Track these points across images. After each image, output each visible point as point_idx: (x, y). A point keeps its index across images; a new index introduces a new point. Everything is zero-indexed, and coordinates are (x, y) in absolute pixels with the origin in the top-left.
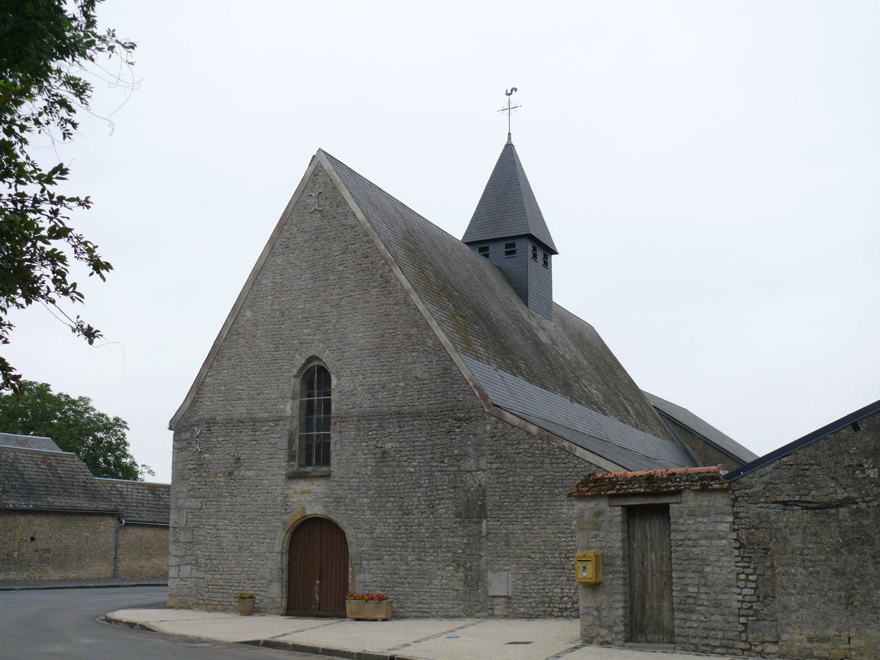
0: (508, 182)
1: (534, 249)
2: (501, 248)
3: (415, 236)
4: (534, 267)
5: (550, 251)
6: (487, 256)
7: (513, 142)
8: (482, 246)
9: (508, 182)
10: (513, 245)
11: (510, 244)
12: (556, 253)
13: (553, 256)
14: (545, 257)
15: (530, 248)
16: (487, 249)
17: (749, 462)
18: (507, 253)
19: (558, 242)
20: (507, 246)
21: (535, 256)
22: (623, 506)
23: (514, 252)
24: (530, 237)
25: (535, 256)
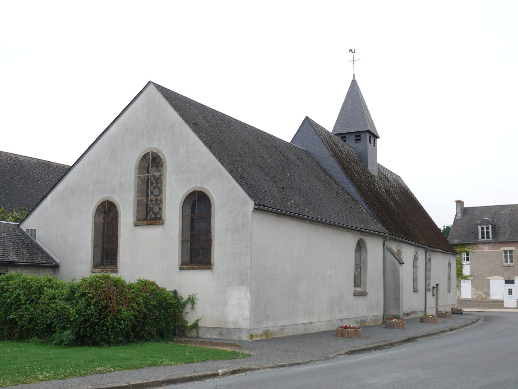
0: (354, 100)
1: (370, 137)
2: (353, 137)
3: (439, 230)
4: (370, 146)
5: (376, 137)
6: (345, 141)
7: (356, 78)
8: (342, 136)
9: (354, 100)
10: (359, 136)
11: (358, 136)
12: (378, 138)
13: (378, 139)
14: (374, 140)
15: (368, 137)
16: (345, 137)
17: (378, 162)
18: (356, 140)
19: (380, 133)
20: (356, 136)
21: (370, 141)
22: (505, 308)
23: (360, 140)
24: (369, 132)
25: (370, 141)
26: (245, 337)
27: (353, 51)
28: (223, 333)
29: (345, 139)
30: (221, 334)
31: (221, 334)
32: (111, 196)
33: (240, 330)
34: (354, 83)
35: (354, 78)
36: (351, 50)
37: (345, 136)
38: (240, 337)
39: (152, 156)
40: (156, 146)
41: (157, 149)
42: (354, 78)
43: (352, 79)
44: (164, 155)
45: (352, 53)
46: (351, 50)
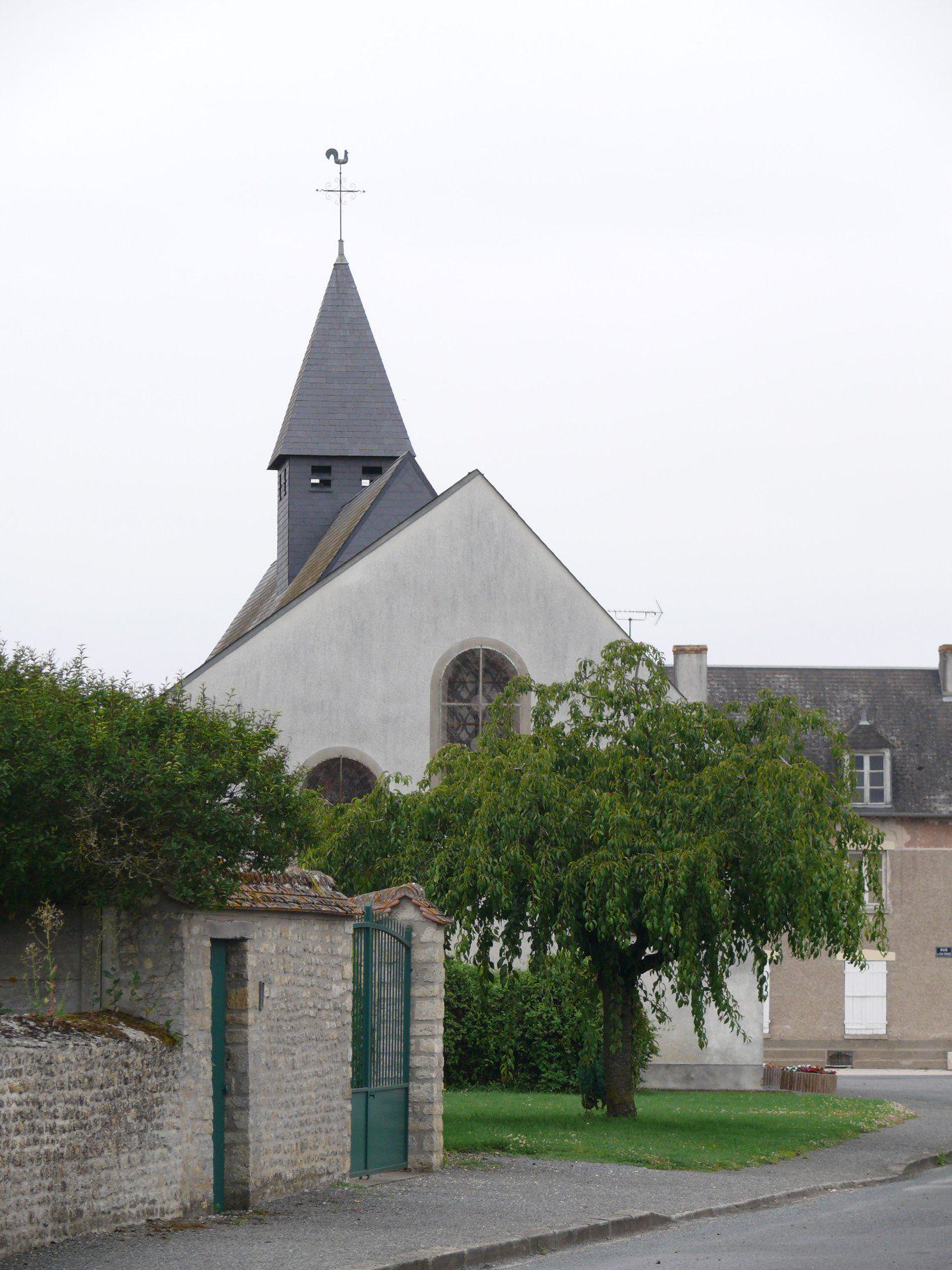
26: (751, 1082)
27: (341, 157)
28: (693, 1075)
29: (326, 477)
30: (688, 1078)
31: (688, 1078)
32: (357, 746)
33: (737, 1068)
34: (342, 279)
35: (341, 254)
36: (331, 152)
37: (327, 463)
38: (737, 1084)
39: (487, 661)
40: (497, 637)
41: (499, 644)
42: (341, 254)
43: (333, 258)
44: (520, 662)
45: (338, 162)
46: (331, 152)
